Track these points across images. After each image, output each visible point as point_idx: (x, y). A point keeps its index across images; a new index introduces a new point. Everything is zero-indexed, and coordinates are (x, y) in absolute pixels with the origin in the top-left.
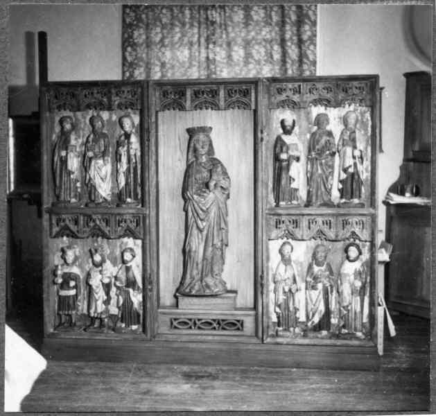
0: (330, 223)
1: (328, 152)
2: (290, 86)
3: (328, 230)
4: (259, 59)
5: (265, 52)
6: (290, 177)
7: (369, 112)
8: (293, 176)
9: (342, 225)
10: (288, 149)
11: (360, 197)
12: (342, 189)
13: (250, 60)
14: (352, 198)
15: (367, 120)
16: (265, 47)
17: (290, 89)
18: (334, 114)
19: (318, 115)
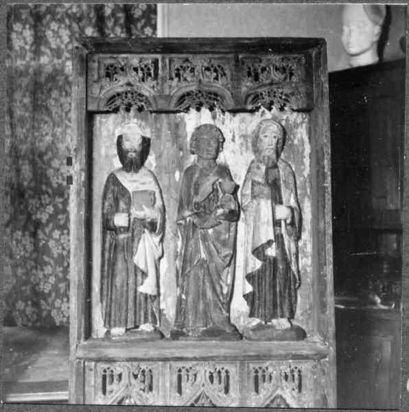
0: (228, 377)
1: (220, 211)
2: (135, 60)
3: (222, 394)
4: (59, 48)
5: (70, 37)
6: (136, 267)
7: (304, 125)
8: (142, 266)
9: (252, 381)
10: (129, 204)
11: (292, 316)
12: (253, 294)
13: (43, 48)
14: (274, 316)
15: (302, 141)
16: (70, 27)
17: (136, 69)
18: (231, 125)
19: (198, 129)
